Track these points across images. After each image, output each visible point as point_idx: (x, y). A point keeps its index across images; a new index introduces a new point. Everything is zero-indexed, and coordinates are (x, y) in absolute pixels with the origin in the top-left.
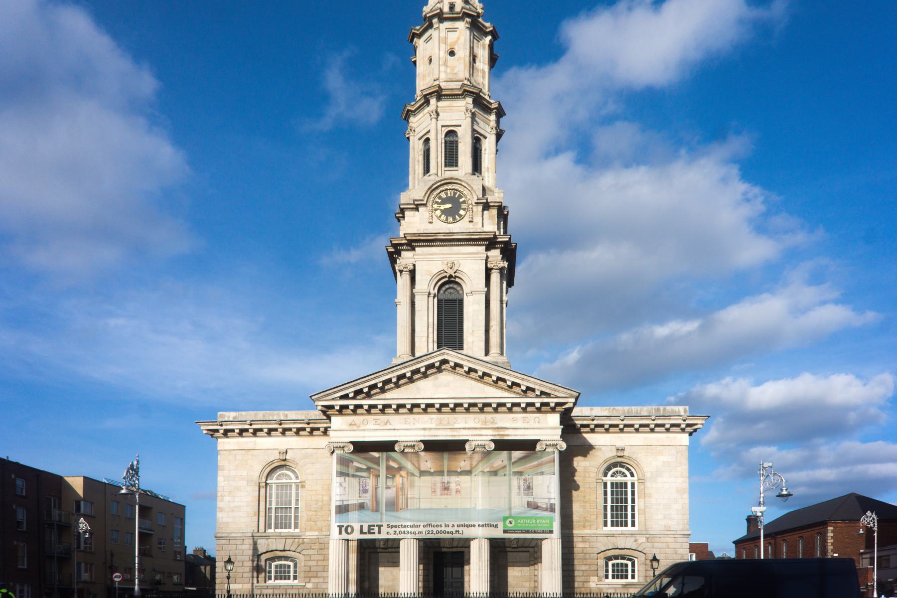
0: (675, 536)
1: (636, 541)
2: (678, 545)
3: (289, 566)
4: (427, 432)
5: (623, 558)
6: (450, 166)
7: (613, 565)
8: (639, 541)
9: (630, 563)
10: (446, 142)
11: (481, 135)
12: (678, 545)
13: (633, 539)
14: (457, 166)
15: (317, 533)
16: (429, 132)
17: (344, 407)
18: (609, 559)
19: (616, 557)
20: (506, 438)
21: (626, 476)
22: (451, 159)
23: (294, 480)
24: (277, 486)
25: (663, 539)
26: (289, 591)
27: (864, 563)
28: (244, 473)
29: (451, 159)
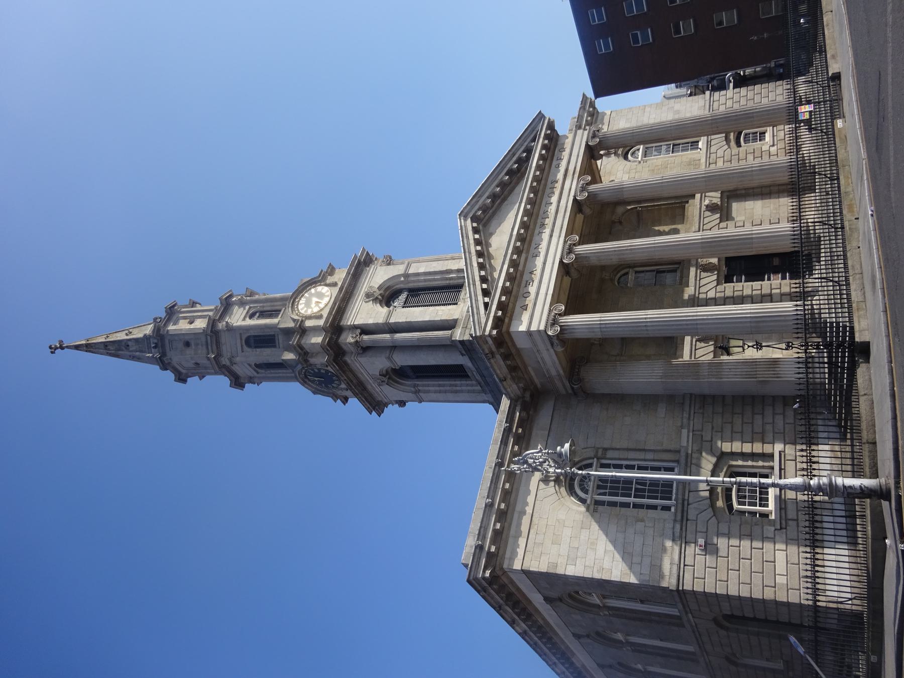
3: (746, 134)
9: (736, 506)
10: (256, 347)
15: (684, 432)
16: (250, 365)
17: (501, 306)
28: (567, 532)
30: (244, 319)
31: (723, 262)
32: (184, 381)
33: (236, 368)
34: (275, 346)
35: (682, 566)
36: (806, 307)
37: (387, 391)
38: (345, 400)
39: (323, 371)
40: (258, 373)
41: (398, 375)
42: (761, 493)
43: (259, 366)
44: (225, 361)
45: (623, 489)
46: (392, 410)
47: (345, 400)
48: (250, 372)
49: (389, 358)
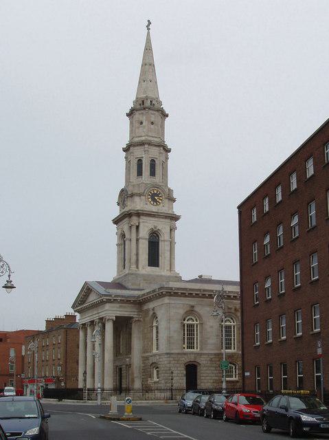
24: (115, 323)
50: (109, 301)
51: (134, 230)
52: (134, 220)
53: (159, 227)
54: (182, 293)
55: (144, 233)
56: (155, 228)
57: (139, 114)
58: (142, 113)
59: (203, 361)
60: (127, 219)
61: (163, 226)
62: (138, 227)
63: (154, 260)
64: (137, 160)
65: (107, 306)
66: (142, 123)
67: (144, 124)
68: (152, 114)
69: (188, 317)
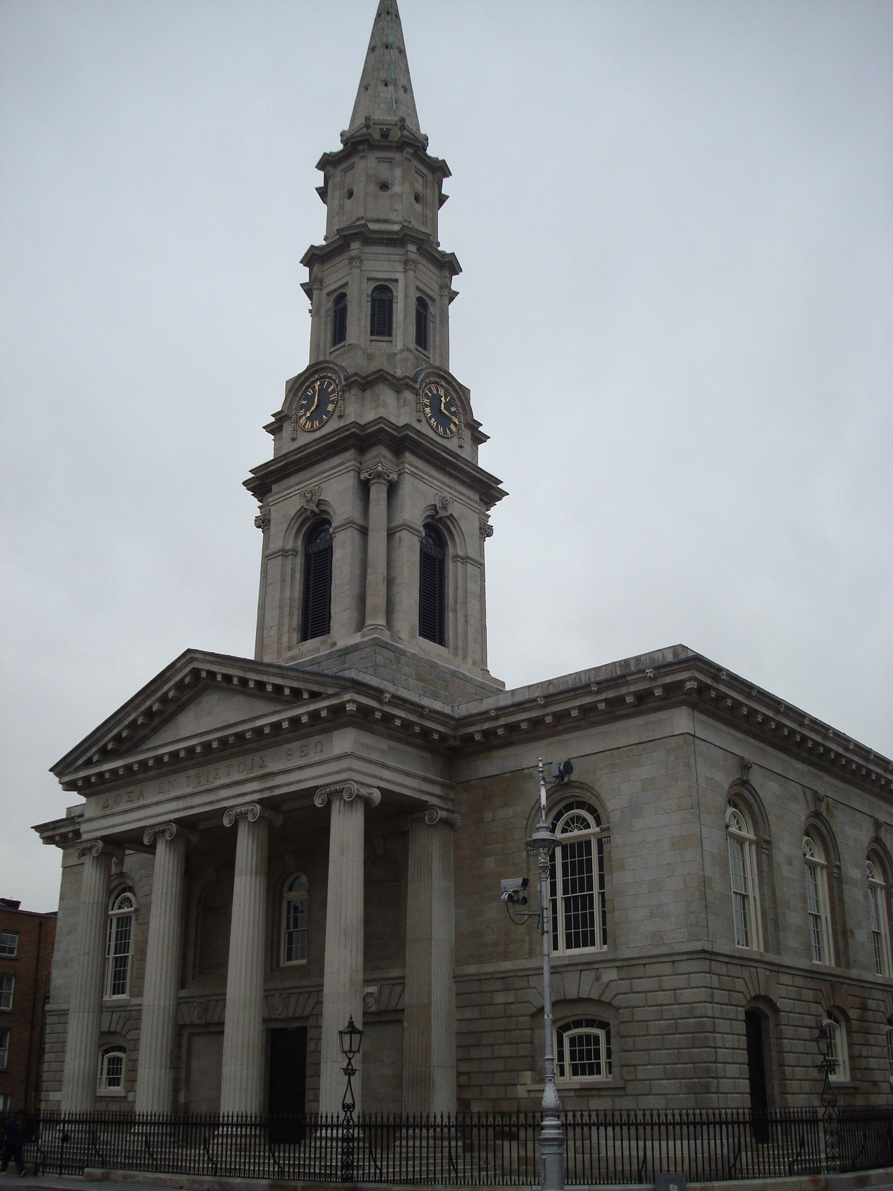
0: (673, 958)
1: (598, 979)
2: (680, 981)
3: (597, 1038)
4: (180, 804)
5: (590, 1023)
6: (379, 334)
7: (572, 1041)
8: (605, 979)
11: (428, 295)
12: (680, 981)
13: (592, 975)
14: (390, 335)
16: (346, 284)
18: (566, 1028)
19: (578, 1024)
20: (277, 792)
21: (588, 826)
22: (381, 324)
23: (594, 829)
24: (118, 919)
25: (652, 970)
26: (98, 1171)
27: (443, 399)
29: (381, 324)
30: (418, 288)
31: (376, 975)
32: (321, 166)
33: (341, 261)
34: (372, 334)
35: (216, 998)
36: (446, 1130)
37: (290, 502)
38: (274, 429)
39: (330, 407)
40: (328, 294)
41: (315, 528)
42: (583, 1065)
43: (340, 299)
44: (355, 246)
45: (581, 1051)
46: (252, 506)
47: (274, 429)
48: (333, 282)
49: (349, 523)
50: (364, 719)
51: (378, 493)
52: (380, 458)
53: (455, 510)
54: (582, 709)
55: (413, 508)
56: (445, 508)
57: (380, 160)
58: (390, 161)
59: (783, 993)
60: (350, 454)
61: (461, 505)
62: (392, 489)
63: (433, 625)
64: (370, 287)
65: (344, 741)
66: (384, 186)
67: (397, 189)
68: (418, 172)
69: (567, 815)
